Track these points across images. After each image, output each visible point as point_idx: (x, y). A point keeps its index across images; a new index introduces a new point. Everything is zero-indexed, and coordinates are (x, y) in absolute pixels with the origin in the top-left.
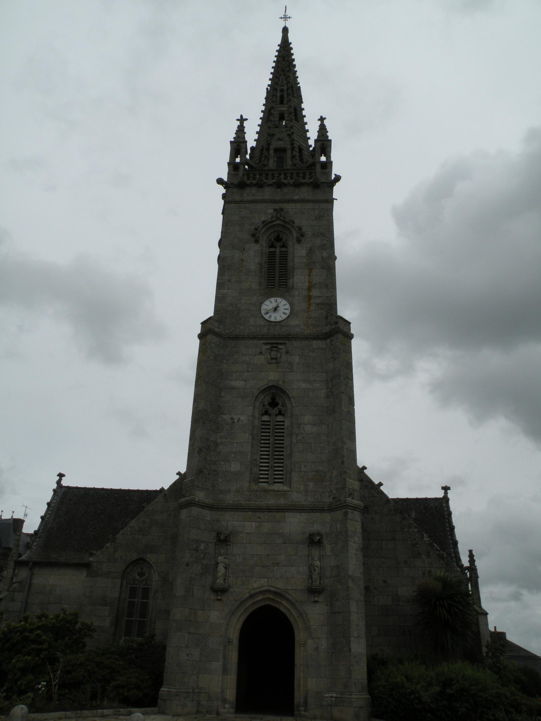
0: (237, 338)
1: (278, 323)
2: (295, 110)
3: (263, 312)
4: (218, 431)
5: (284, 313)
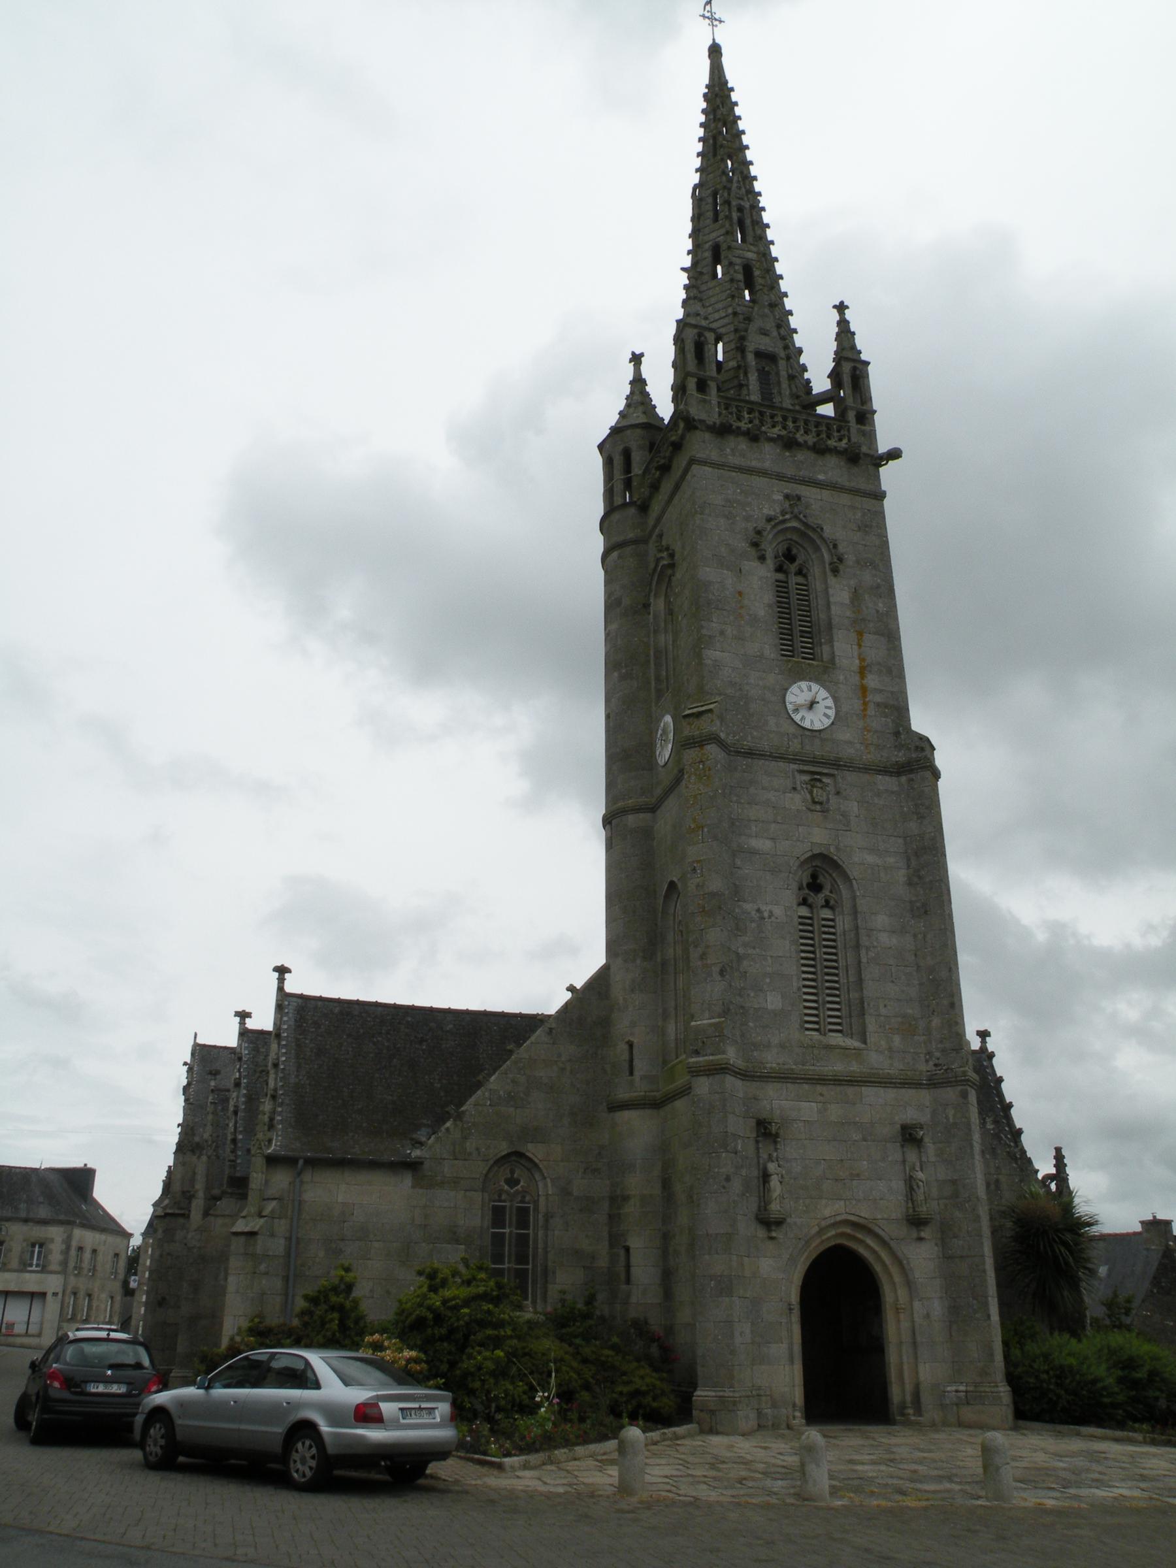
0: (750, 754)
1: (817, 734)
3: (790, 707)
4: (739, 934)
5: (826, 715)
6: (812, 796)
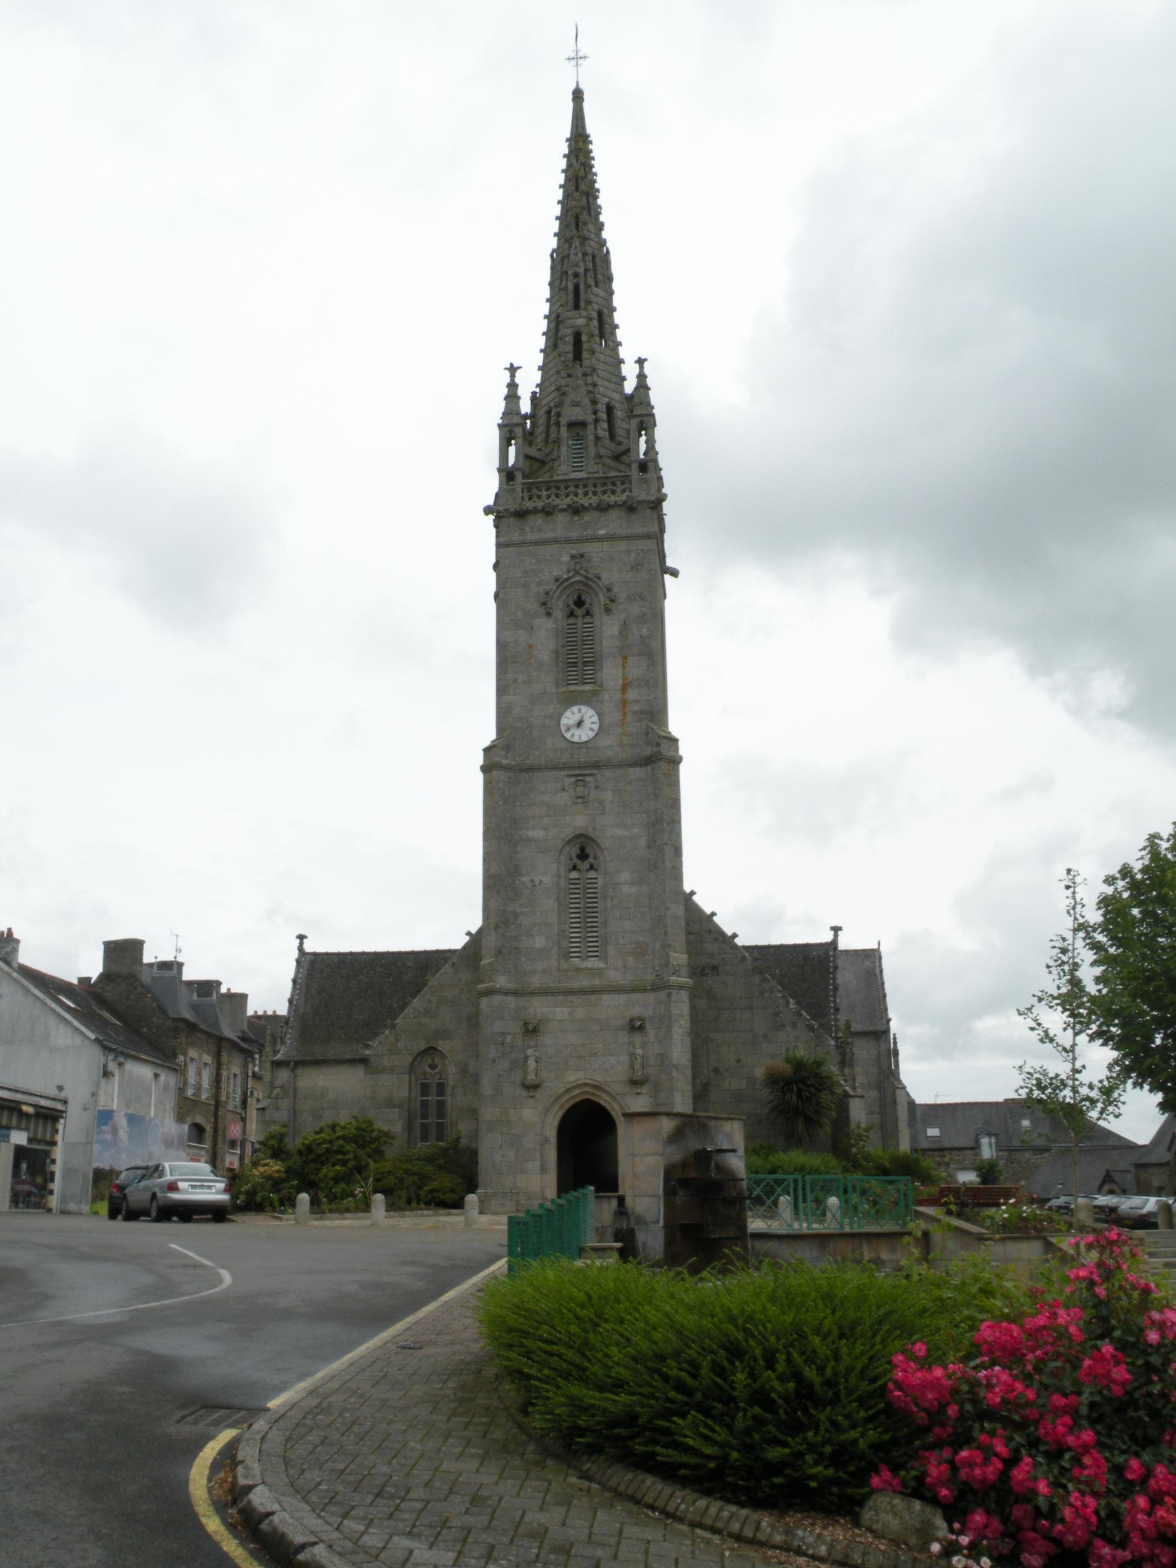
0: (531, 769)
2: (600, 314)
3: (563, 728)
5: (591, 729)
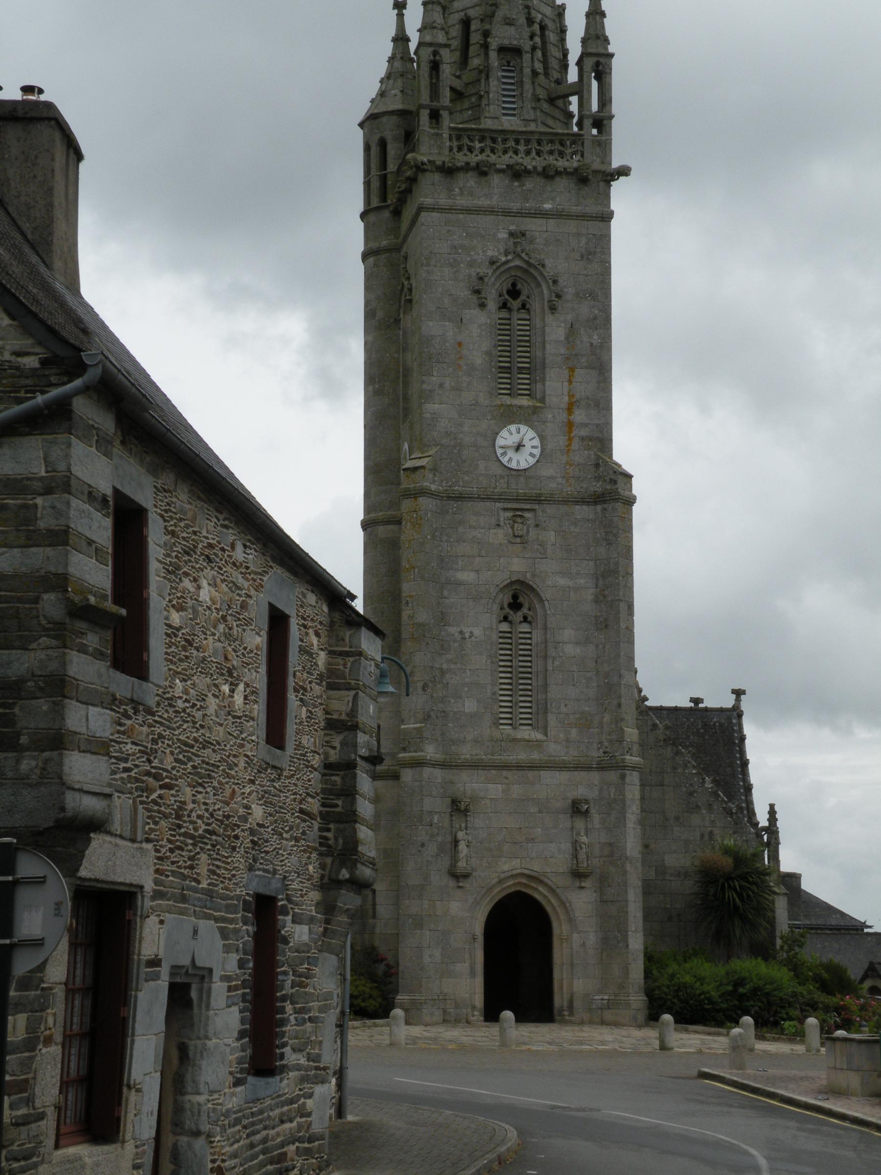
0: (460, 498)
3: (499, 451)
4: (443, 652)
6: (513, 530)
